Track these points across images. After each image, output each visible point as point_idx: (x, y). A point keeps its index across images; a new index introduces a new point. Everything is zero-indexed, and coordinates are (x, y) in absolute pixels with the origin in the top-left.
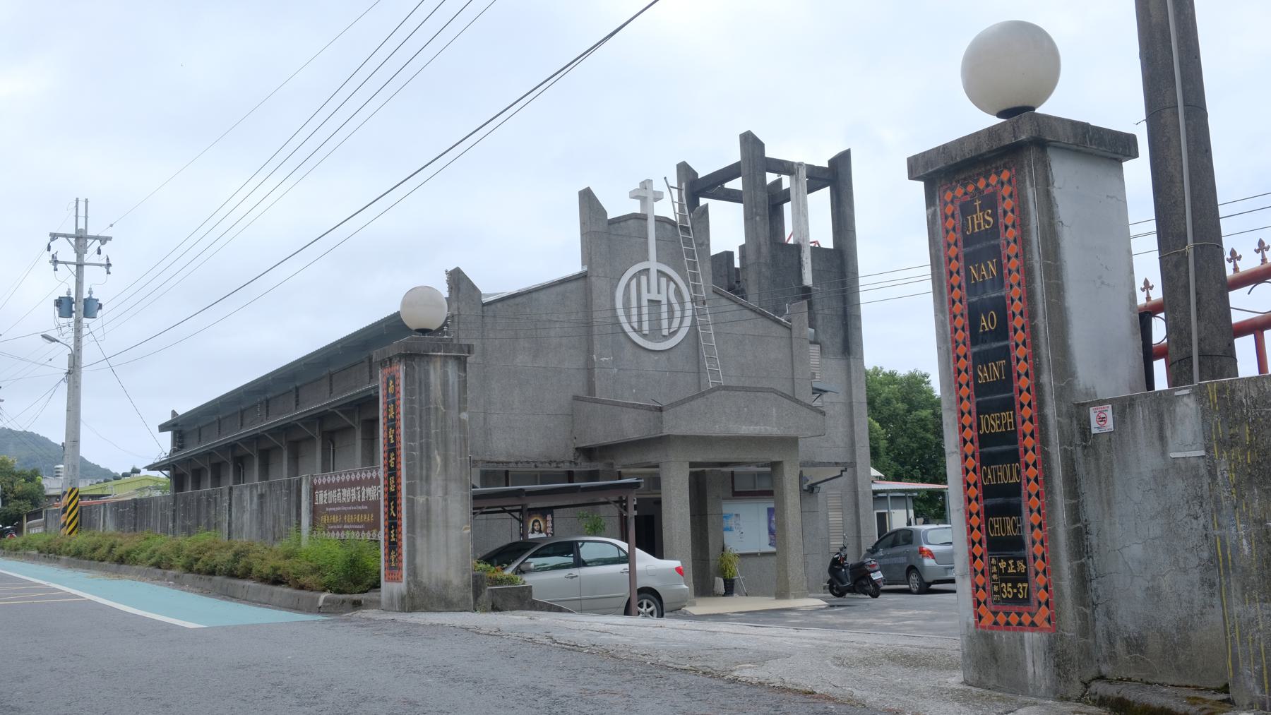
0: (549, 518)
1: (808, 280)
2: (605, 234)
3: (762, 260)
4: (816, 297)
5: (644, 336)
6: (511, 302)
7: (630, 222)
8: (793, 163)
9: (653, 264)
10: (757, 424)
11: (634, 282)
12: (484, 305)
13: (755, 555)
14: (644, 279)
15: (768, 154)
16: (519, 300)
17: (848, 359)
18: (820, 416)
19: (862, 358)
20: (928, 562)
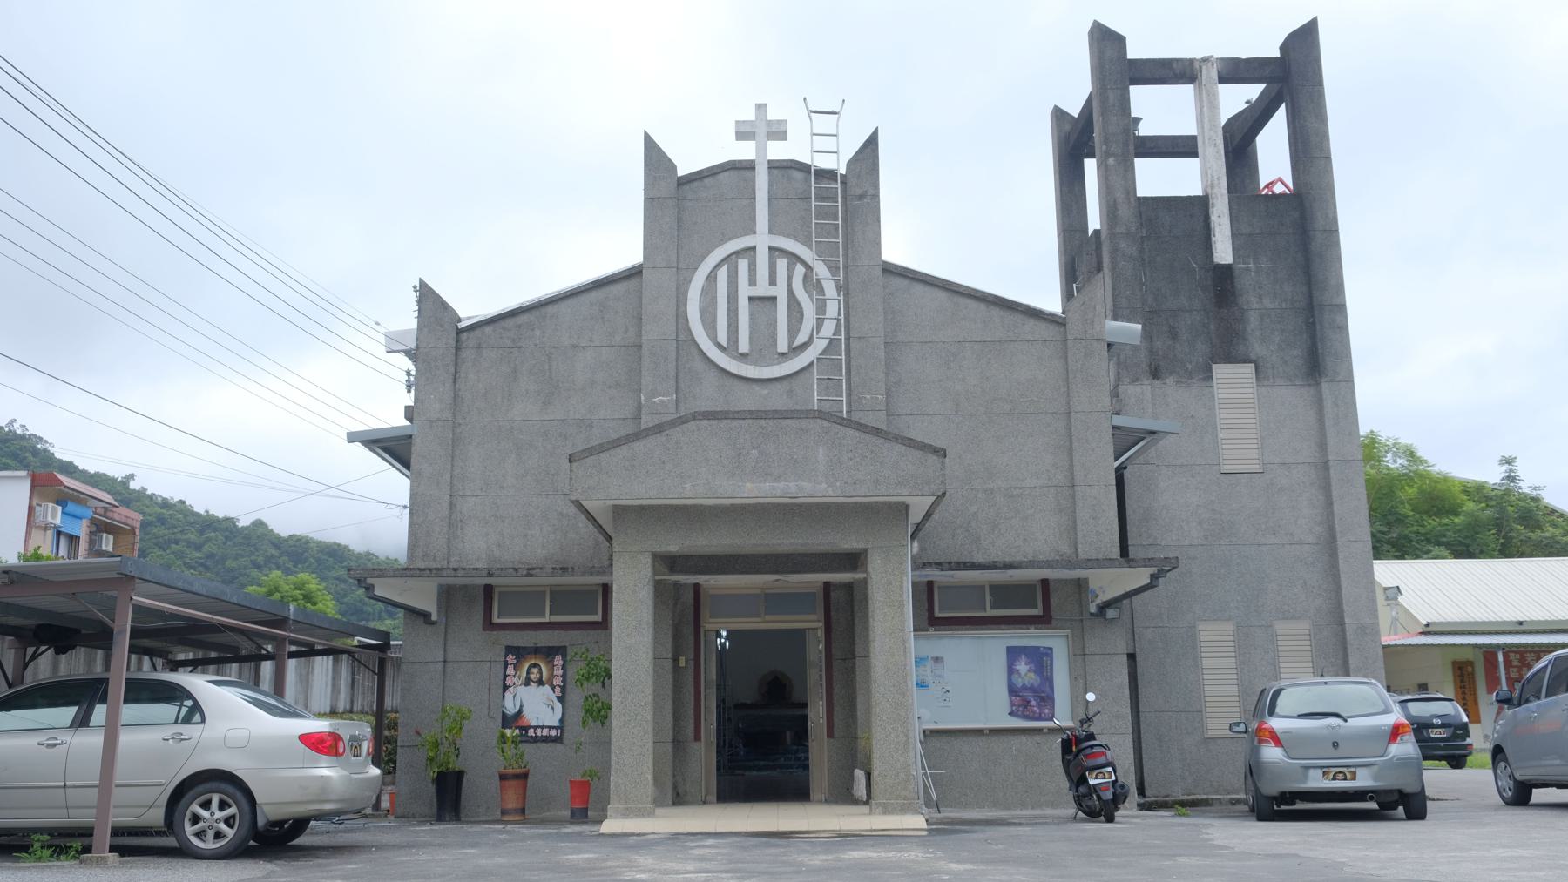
0: (558, 661)
1: (1223, 253)
2: (684, 201)
3: (1121, 229)
4: (1245, 283)
5: (743, 357)
6: (510, 323)
7: (721, 176)
8: (1191, 61)
9: (762, 240)
10: (778, 478)
11: (723, 274)
12: (460, 332)
13: (979, 732)
14: (743, 265)
15: (1132, 54)
16: (523, 318)
17: (1318, 384)
18: (933, 459)
19: (1349, 380)
20: (1271, 753)
